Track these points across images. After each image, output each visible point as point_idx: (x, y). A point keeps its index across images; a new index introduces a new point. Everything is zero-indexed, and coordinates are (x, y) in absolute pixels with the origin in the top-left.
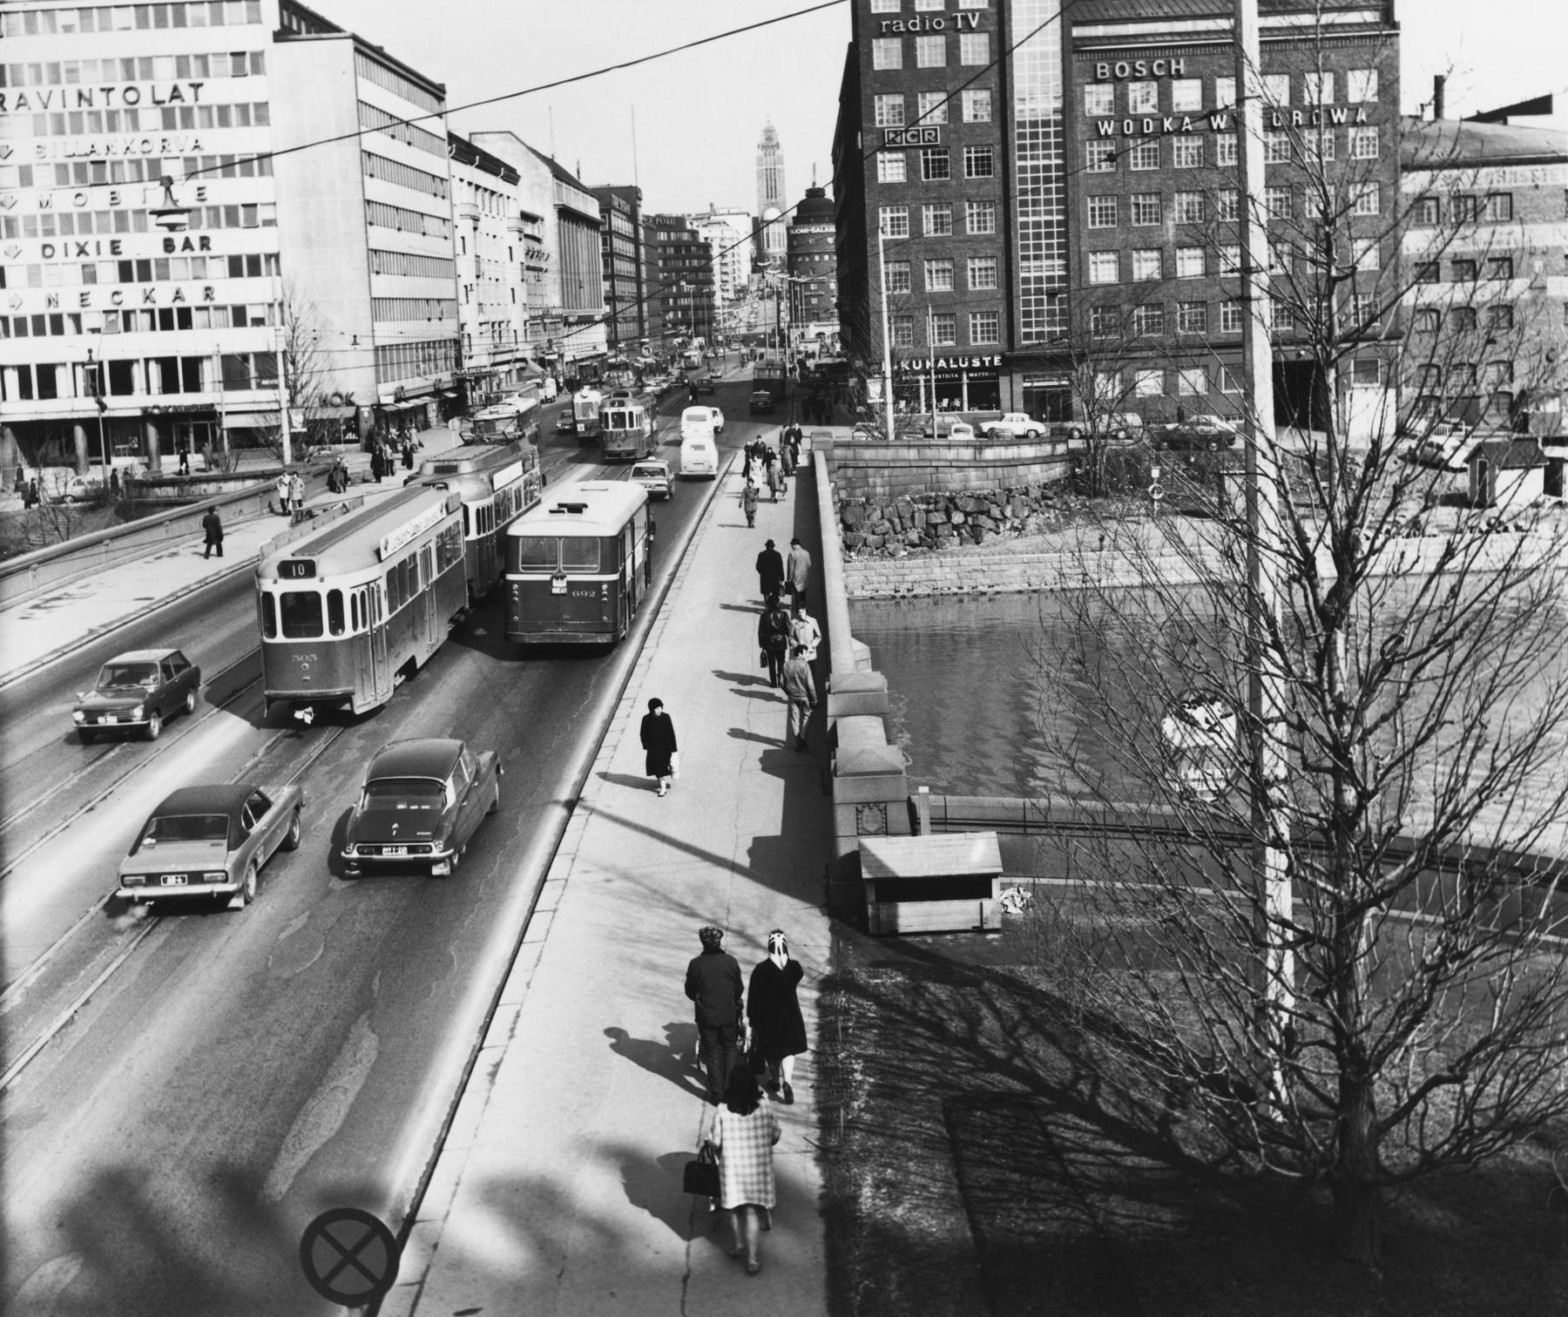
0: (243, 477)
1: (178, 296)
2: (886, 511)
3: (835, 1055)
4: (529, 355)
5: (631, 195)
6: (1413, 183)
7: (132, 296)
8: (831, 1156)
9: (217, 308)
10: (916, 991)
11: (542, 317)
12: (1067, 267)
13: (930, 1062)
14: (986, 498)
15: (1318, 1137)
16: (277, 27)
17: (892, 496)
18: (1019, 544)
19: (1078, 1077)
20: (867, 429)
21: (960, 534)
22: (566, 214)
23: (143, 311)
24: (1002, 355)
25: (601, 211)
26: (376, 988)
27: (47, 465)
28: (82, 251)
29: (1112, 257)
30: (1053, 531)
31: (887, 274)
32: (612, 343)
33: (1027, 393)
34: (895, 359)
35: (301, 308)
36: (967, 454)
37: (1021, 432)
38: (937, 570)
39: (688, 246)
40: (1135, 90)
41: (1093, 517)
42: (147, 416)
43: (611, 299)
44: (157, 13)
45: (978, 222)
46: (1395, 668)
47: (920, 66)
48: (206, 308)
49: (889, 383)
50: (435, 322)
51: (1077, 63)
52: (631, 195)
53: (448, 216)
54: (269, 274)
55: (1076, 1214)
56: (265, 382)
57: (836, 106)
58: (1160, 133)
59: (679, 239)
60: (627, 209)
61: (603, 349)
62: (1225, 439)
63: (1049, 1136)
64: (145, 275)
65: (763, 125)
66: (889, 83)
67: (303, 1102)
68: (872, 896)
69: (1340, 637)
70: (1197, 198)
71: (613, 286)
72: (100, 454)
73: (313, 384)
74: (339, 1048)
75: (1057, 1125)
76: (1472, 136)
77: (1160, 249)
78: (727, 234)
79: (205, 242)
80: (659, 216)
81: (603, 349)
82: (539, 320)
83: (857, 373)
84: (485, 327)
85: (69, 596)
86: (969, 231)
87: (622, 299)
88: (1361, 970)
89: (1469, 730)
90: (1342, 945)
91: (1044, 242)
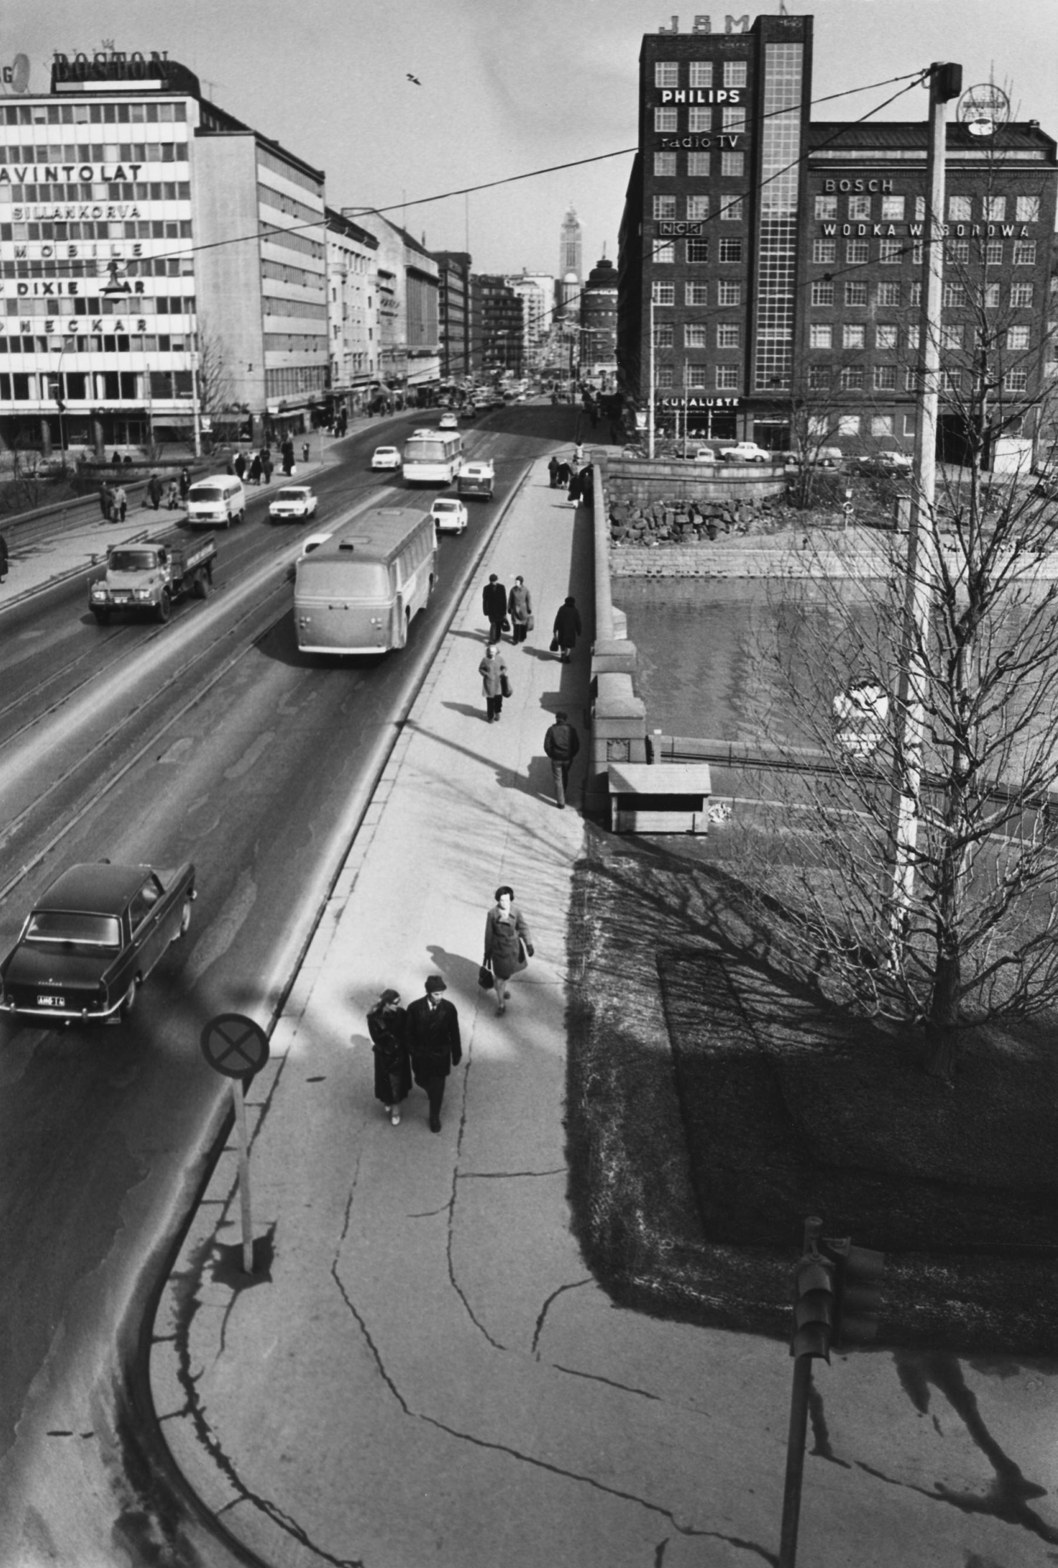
0: (165, 465)
1: (119, 326)
2: (645, 512)
3: (582, 916)
5: (464, 260)
7: (85, 324)
9: (148, 336)
10: (646, 874)
11: (392, 351)
12: (793, 335)
14: (720, 506)
15: (921, 994)
17: (650, 501)
18: (743, 541)
20: (632, 449)
23: (93, 337)
25: (440, 271)
28: (48, 289)
29: (828, 329)
31: (655, 332)
32: (445, 373)
34: (658, 398)
36: (708, 472)
37: (750, 457)
38: (680, 558)
39: (505, 300)
40: (854, 201)
41: (803, 524)
42: (95, 415)
43: (445, 338)
45: (729, 297)
49: (652, 415)
50: (311, 352)
51: (811, 180)
52: (464, 260)
54: (187, 312)
57: (623, 201)
58: (871, 234)
59: (498, 295)
60: (459, 270)
61: (437, 376)
62: (902, 471)
63: (730, 980)
64: (94, 311)
66: (665, 186)
68: (614, 805)
69: (968, 649)
71: (446, 330)
73: (218, 398)
75: (737, 973)
77: (864, 325)
78: (535, 291)
79: (140, 287)
80: (485, 276)
81: (437, 376)
82: (390, 354)
83: (629, 405)
84: (348, 358)
85: (36, 550)
86: (720, 304)
87: (453, 339)
90: (947, 866)
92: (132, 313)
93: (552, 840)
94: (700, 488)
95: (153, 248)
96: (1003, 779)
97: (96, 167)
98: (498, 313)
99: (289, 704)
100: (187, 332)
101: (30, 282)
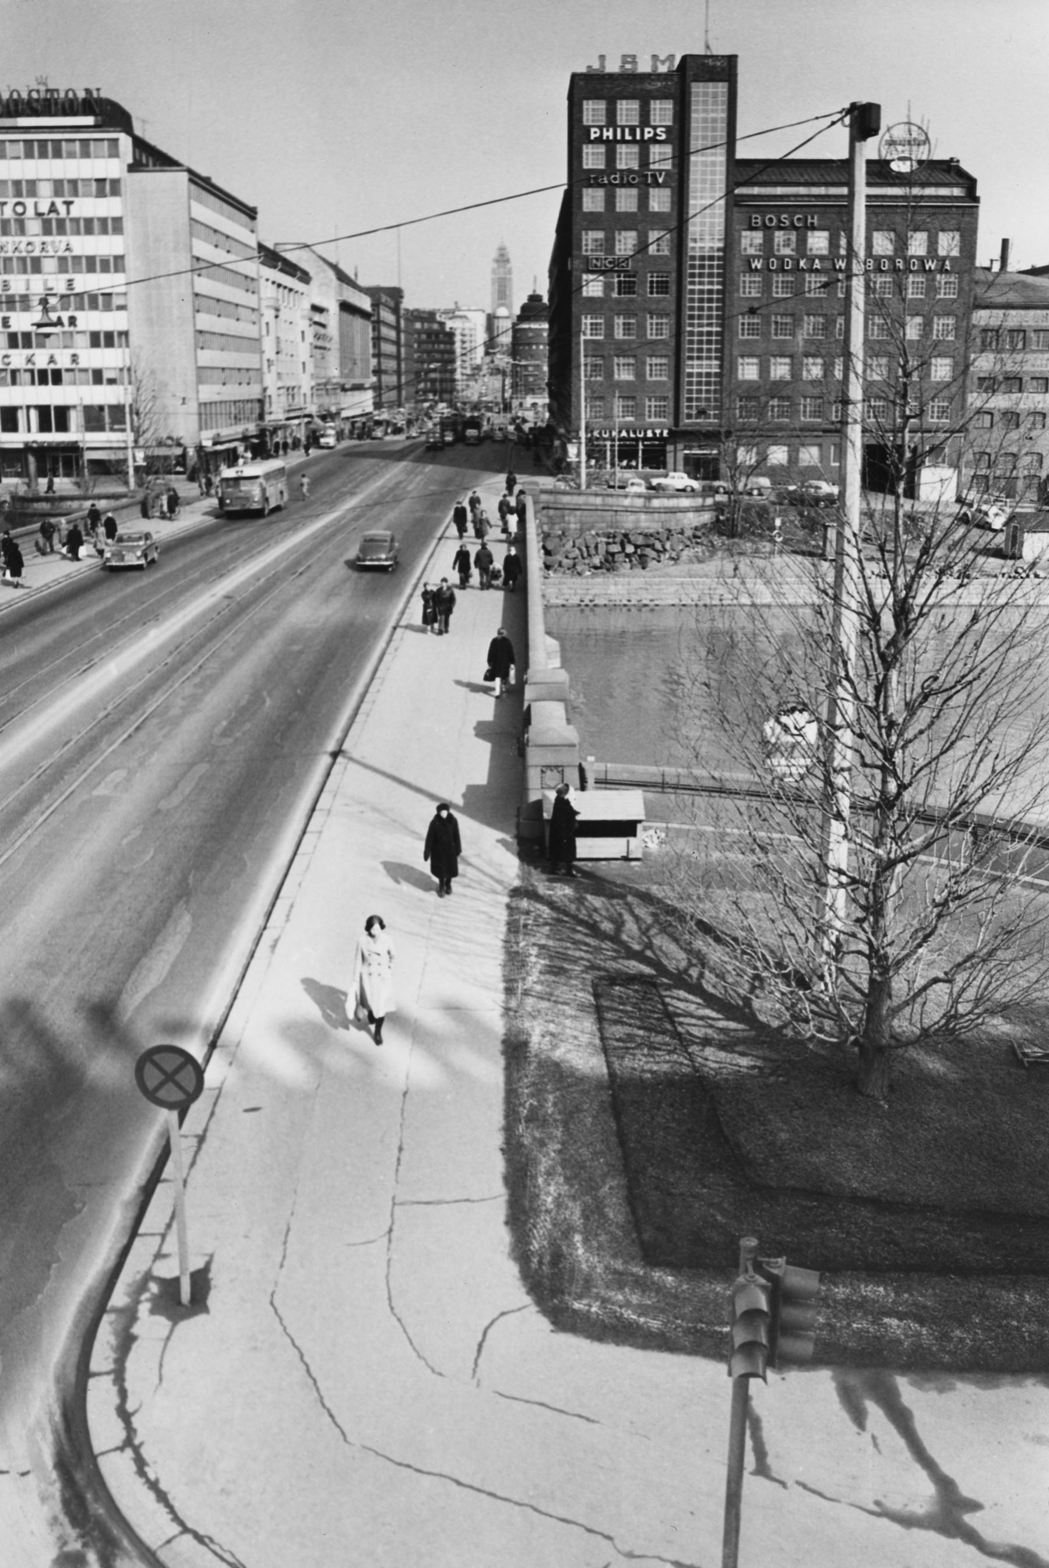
1: (52, 360)
2: (578, 542)
3: (517, 943)
5: (396, 294)
6: (982, 317)
8: (511, 1013)
9: (81, 370)
11: (325, 384)
12: (721, 367)
13: (586, 952)
15: (853, 1014)
16: (130, 160)
17: (582, 531)
18: (673, 570)
19: (691, 965)
22: (346, 307)
23: (26, 370)
25: (373, 305)
29: (755, 360)
30: (700, 561)
32: (378, 405)
34: (589, 429)
36: (640, 502)
37: (681, 487)
38: (613, 588)
39: (437, 334)
40: (779, 236)
42: (28, 449)
43: (378, 372)
44: (40, 147)
46: (930, 699)
47: (618, 210)
50: (244, 385)
51: (738, 215)
52: (396, 294)
53: (255, 306)
54: (120, 346)
55: (681, 1059)
59: (430, 328)
60: (392, 304)
61: (370, 408)
62: (830, 499)
63: (665, 1005)
64: (28, 344)
65: (496, 246)
66: (594, 221)
67: (139, 959)
69: (894, 674)
70: (821, 320)
71: (379, 363)
73: (152, 430)
74: (165, 923)
76: (1025, 285)
77: (791, 356)
79: (72, 321)
80: (417, 310)
81: (370, 408)
82: (323, 387)
83: (560, 437)
84: (282, 391)
87: (385, 372)
88: (890, 905)
89: (979, 744)
94: (632, 517)
95: (87, 282)
97: (29, 202)
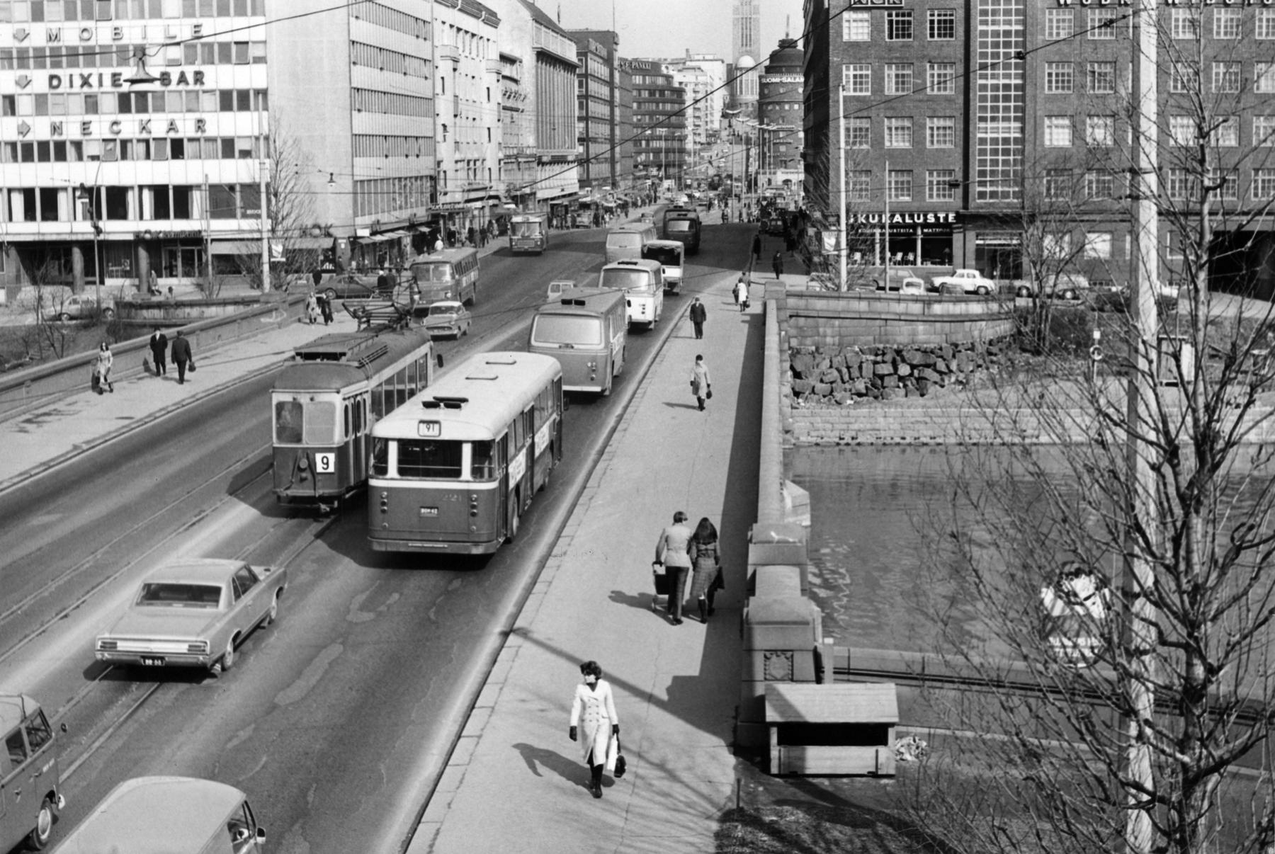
0: (224, 303)
1: (172, 127)
2: (835, 360)
4: (502, 193)
5: (609, 39)
7: (130, 125)
9: (208, 140)
11: (516, 157)
12: (1023, 130)
14: (932, 352)
21: (905, 386)
22: (544, 57)
23: (139, 141)
24: (957, 213)
25: (579, 54)
26: (310, 799)
27: (47, 283)
28: (86, 82)
29: (1066, 122)
31: (848, 130)
32: (583, 183)
33: (980, 251)
35: (285, 143)
36: (916, 308)
37: (971, 288)
38: (881, 420)
42: (140, 240)
48: (198, 140)
49: (843, 235)
52: (609, 39)
53: (429, 57)
54: (257, 109)
56: (249, 212)
61: (574, 187)
68: (774, 739)
72: (94, 275)
73: (293, 216)
79: (199, 77)
80: (636, 60)
81: (574, 187)
82: (513, 160)
84: (460, 165)
85: (58, 412)
87: (595, 140)
91: (1001, 104)
92: (189, 111)
93: (694, 783)
94: (905, 328)
96: (1242, 691)
98: (653, 107)
99: (363, 608)
100: (256, 133)
101: (63, 73)
